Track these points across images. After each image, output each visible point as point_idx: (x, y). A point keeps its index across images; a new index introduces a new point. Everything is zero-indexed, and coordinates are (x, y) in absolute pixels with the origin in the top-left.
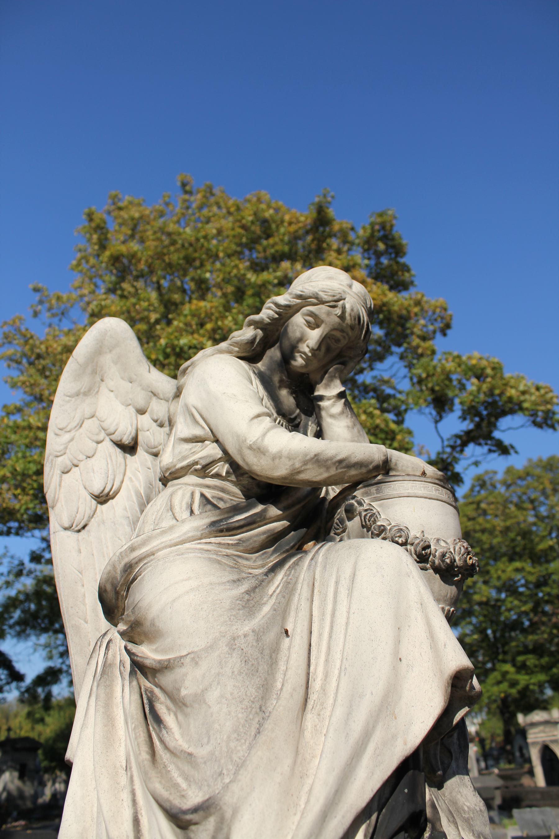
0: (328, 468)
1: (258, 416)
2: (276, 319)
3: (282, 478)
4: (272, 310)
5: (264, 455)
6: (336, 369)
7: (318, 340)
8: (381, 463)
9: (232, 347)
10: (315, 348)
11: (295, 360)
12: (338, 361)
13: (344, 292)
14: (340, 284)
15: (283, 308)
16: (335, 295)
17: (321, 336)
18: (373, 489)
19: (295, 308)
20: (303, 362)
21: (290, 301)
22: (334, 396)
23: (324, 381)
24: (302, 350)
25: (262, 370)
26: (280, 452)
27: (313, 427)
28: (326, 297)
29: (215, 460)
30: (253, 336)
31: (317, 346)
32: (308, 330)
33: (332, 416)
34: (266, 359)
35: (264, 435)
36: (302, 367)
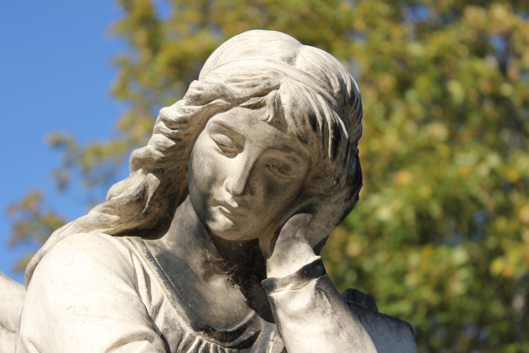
1: (122, 342)
2: (172, 148)
4: (162, 133)
6: (295, 224)
7: (242, 175)
9: (106, 215)
10: (240, 190)
11: (214, 220)
12: (298, 208)
13: (275, 73)
14: (269, 61)
15: (177, 126)
16: (256, 83)
17: (246, 166)
19: (196, 122)
20: (228, 220)
21: (184, 111)
22: (291, 277)
23: (276, 251)
24: (219, 199)
25: (168, 248)
27: (276, 343)
28: (239, 90)
30: (139, 187)
31: (242, 186)
32: (223, 159)
33: (293, 317)
34: (174, 227)
36: (227, 231)
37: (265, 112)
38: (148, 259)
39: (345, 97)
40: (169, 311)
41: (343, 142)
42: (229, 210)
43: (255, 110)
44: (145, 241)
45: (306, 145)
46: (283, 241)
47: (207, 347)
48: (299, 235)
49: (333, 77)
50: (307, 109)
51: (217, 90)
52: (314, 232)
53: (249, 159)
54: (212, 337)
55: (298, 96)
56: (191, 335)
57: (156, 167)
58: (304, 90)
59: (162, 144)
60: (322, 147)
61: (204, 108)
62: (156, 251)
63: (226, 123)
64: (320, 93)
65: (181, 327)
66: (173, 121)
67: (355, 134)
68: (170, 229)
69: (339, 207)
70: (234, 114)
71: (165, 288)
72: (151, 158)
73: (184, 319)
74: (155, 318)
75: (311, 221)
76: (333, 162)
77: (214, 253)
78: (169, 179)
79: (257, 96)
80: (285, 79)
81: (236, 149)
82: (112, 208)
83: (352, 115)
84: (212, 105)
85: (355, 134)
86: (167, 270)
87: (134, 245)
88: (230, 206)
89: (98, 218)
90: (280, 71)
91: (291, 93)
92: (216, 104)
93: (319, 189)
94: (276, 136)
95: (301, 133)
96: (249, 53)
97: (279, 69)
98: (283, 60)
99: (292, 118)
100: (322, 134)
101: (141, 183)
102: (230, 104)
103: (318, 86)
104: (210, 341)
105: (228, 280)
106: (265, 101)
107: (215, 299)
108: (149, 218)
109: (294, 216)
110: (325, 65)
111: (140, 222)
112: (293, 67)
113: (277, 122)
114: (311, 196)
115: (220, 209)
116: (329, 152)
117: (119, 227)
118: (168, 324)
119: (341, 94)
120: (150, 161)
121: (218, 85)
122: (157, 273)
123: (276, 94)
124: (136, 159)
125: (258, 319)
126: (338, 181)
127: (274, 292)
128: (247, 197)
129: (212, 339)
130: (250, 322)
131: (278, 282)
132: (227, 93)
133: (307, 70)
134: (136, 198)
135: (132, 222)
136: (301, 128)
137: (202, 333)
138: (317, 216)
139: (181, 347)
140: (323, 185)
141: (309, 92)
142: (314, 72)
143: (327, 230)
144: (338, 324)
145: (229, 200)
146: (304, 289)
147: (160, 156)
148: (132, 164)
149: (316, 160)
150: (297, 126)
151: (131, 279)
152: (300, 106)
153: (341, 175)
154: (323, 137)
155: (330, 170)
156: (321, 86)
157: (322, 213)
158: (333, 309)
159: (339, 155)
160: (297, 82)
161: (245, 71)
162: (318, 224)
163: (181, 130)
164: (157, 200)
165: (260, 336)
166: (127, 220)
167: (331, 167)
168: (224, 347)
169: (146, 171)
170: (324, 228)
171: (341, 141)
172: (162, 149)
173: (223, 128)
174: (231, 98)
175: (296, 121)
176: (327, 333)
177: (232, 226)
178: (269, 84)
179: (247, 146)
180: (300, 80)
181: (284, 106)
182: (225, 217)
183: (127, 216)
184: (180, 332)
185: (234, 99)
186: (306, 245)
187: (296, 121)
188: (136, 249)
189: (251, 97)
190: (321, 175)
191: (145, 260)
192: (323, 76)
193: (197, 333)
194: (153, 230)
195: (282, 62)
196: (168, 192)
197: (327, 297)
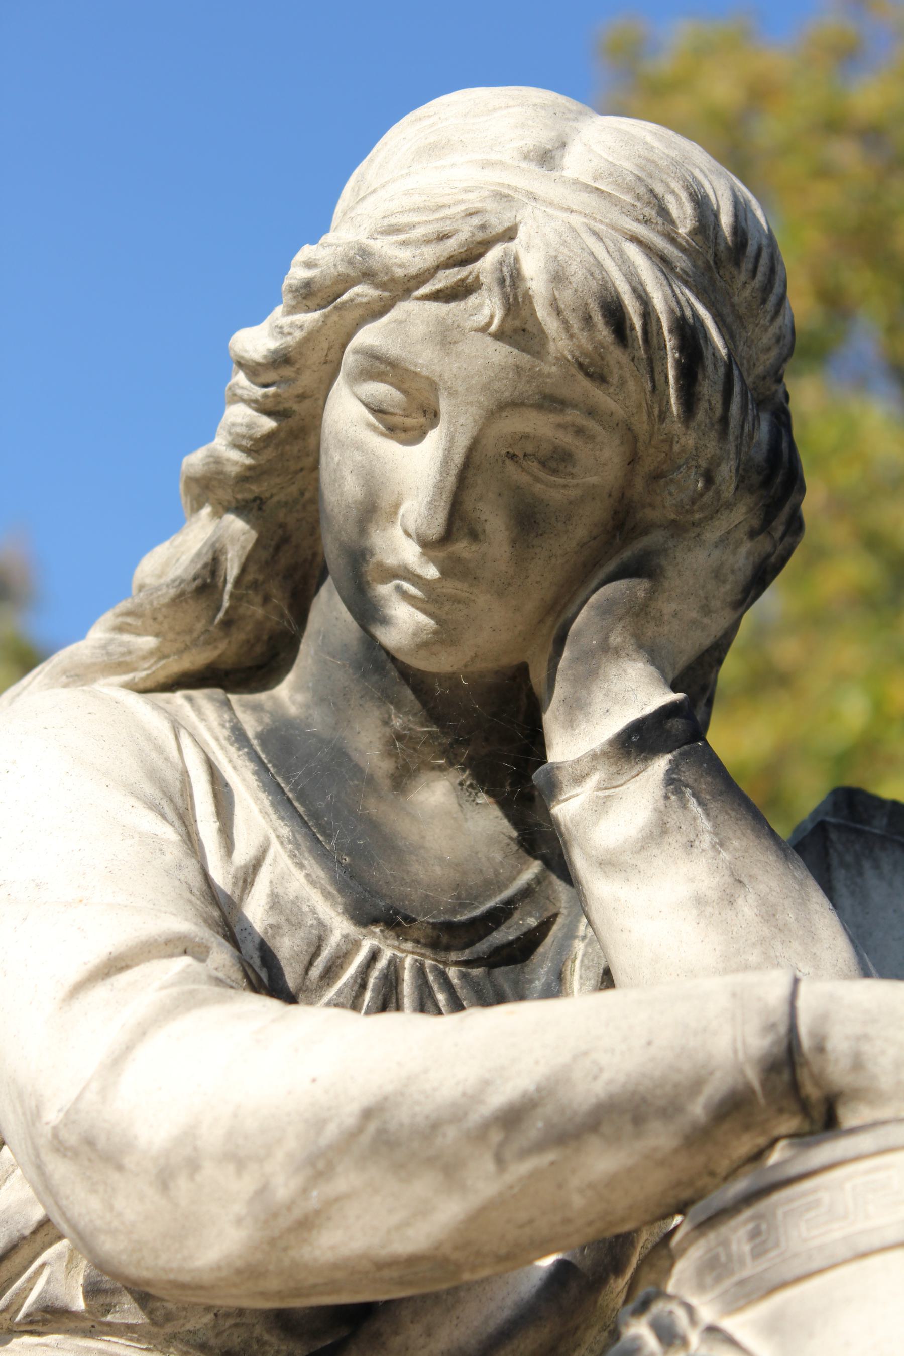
0: (450, 1170)
1: (115, 966)
2: (270, 437)
3: (239, 1272)
4: (243, 400)
5: (120, 1168)
6: (606, 609)
7: (439, 489)
8: (753, 1076)
9: (126, 638)
10: (435, 530)
11: (385, 621)
12: (611, 566)
13: (503, 197)
14: (487, 164)
15: (271, 376)
16: (447, 227)
17: (446, 461)
18: (737, 1234)
19: (314, 357)
20: (422, 618)
21: (280, 331)
23: (559, 691)
24: (391, 561)
25: (293, 710)
26: (189, 1135)
28: (404, 254)
29: (23, 1238)
30: (199, 555)
31: (441, 518)
32: (391, 450)
33: (608, 864)
34: (307, 649)
35: (117, 1061)
37: (480, 306)
38: (232, 745)
39: (716, 244)
40: (283, 878)
41: (710, 368)
42: (419, 589)
43: (453, 305)
44: (233, 698)
45: (605, 385)
46: (575, 660)
47: (394, 968)
48: (619, 640)
49: (673, 192)
50: (594, 285)
51: (350, 262)
52: (665, 629)
53: (451, 440)
54: (406, 940)
55: (566, 251)
56: (346, 936)
57: (239, 496)
58: (584, 235)
59: (242, 430)
60: (649, 386)
61: (326, 317)
62: (260, 721)
63: (384, 350)
64: (635, 239)
65: (318, 919)
66: (258, 364)
67: (769, 349)
68: (298, 661)
69: (734, 553)
70: (401, 322)
71: (274, 817)
72: (221, 472)
73: (327, 895)
74: (241, 899)
75: (651, 599)
76: (687, 427)
77: (415, 715)
78: (282, 526)
79: (454, 266)
80: (530, 209)
81: (422, 420)
82: (135, 620)
83: (747, 293)
84: (344, 304)
85: (769, 349)
86: (287, 771)
87: (198, 711)
88: (420, 577)
89: (104, 647)
90: (516, 190)
91: (548, 245)
92: (352, 300)
93: (664, 507)
94: (518, 369)
95: (585, 354)
96: (434, 150)
97: (513, 184)
98: (526, 157)
99: (554, 314)
100: (646, 351)
101: (205, 544)
102: (386, 294)
103: (628, 220)
104: (403, 951)
105: (461, 784)
106: (477, 277)
107: (423, 837)
108: (239, 636)
109: (602, 590)
110: (648, 160)
111: (216, 648)
112: (555, 174)
113: (515, 331)
114: (647, 529)
115: (398, 588)
116: (673, 400)
117: (163, 668)
118: (281, 912)
119: (699, 237)
120: (220, 481)
121: (351, 248)
122: (254, 778)
123: (506, 254)
124: (192, 480)
125: (551, 883)
126: (709, 479)
127: (559, 802)
128: (461, 547)
129: (409, 946)
130: (527, 893)
131: (564, 773)
132: (375, 264)
133: (595, 179)
134: (194, 585)
135: (194, 651)
136: (583, 341)
137: (377, 930)
138: (666, 584)
139: (316, 972)
140: (671, 494)
141: (600, 238)
142: (615, 183)
143: (706, 621)
144: (732, 874)
145: (416, 559)
146: (633, 786)
147: (243, 465)
148: (186, 495)
149: (645, 427)
150: (572, 337)
151: (171, 800)
152: (573, 279)
153: (715, 462)
154: (650, 361)
155: (683, 449)
156: (638, 220)
157: (680, 574)
158: (716, 834)
159: (703, 406)
160: (565, 215)
161: (418, 200)
162: (674, 606)
163: (283, 385)
164: (255, 585)
165: (555, 928)
166: (179, 645)
167: (683, 440)
168: (446, 964)
169: (221, 510)
170: (694, 614)
171: (704, 368)
172: (244, 443)
173: (377, 363)
174: (386, 278)
175: (565, 322)
176: (699, 901)
177: (435, 633)
178: (483, 227)
179: (444, 406)
180: (574, 207)
181: (529, 284)
182: (413, 610)
183: (178, 634)
184: (315, 932)
185: (393, 280)
186: (640, 665)
187: (565, 322)
188: (203, 719)
189: (438, 268)
190: (664, 467)
191: (222, 748)
192: (642, 190)
193: (363, 930)
194: (259, 668)
195: (524, 165)
196: (284, 560)
197: (701, 803)
